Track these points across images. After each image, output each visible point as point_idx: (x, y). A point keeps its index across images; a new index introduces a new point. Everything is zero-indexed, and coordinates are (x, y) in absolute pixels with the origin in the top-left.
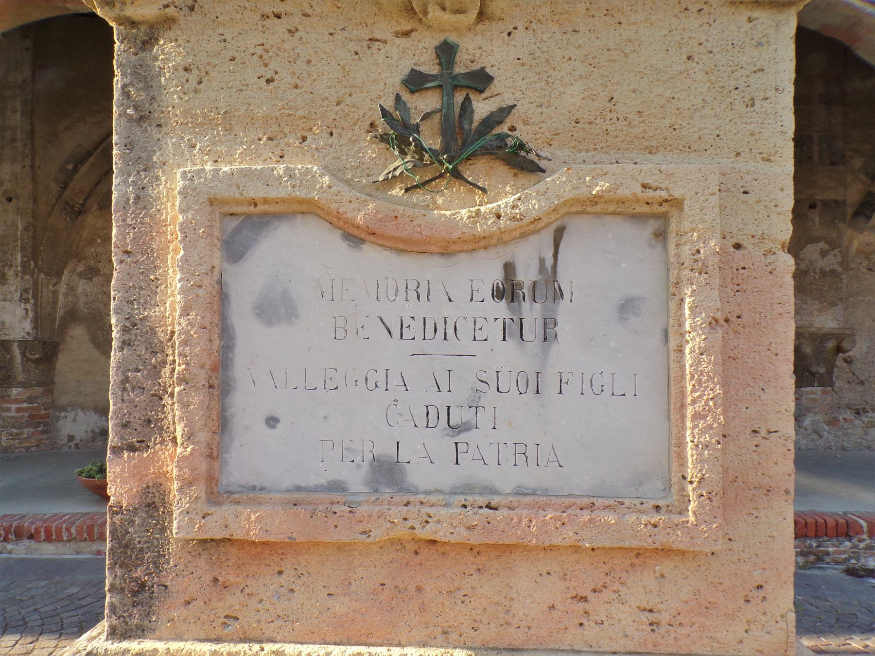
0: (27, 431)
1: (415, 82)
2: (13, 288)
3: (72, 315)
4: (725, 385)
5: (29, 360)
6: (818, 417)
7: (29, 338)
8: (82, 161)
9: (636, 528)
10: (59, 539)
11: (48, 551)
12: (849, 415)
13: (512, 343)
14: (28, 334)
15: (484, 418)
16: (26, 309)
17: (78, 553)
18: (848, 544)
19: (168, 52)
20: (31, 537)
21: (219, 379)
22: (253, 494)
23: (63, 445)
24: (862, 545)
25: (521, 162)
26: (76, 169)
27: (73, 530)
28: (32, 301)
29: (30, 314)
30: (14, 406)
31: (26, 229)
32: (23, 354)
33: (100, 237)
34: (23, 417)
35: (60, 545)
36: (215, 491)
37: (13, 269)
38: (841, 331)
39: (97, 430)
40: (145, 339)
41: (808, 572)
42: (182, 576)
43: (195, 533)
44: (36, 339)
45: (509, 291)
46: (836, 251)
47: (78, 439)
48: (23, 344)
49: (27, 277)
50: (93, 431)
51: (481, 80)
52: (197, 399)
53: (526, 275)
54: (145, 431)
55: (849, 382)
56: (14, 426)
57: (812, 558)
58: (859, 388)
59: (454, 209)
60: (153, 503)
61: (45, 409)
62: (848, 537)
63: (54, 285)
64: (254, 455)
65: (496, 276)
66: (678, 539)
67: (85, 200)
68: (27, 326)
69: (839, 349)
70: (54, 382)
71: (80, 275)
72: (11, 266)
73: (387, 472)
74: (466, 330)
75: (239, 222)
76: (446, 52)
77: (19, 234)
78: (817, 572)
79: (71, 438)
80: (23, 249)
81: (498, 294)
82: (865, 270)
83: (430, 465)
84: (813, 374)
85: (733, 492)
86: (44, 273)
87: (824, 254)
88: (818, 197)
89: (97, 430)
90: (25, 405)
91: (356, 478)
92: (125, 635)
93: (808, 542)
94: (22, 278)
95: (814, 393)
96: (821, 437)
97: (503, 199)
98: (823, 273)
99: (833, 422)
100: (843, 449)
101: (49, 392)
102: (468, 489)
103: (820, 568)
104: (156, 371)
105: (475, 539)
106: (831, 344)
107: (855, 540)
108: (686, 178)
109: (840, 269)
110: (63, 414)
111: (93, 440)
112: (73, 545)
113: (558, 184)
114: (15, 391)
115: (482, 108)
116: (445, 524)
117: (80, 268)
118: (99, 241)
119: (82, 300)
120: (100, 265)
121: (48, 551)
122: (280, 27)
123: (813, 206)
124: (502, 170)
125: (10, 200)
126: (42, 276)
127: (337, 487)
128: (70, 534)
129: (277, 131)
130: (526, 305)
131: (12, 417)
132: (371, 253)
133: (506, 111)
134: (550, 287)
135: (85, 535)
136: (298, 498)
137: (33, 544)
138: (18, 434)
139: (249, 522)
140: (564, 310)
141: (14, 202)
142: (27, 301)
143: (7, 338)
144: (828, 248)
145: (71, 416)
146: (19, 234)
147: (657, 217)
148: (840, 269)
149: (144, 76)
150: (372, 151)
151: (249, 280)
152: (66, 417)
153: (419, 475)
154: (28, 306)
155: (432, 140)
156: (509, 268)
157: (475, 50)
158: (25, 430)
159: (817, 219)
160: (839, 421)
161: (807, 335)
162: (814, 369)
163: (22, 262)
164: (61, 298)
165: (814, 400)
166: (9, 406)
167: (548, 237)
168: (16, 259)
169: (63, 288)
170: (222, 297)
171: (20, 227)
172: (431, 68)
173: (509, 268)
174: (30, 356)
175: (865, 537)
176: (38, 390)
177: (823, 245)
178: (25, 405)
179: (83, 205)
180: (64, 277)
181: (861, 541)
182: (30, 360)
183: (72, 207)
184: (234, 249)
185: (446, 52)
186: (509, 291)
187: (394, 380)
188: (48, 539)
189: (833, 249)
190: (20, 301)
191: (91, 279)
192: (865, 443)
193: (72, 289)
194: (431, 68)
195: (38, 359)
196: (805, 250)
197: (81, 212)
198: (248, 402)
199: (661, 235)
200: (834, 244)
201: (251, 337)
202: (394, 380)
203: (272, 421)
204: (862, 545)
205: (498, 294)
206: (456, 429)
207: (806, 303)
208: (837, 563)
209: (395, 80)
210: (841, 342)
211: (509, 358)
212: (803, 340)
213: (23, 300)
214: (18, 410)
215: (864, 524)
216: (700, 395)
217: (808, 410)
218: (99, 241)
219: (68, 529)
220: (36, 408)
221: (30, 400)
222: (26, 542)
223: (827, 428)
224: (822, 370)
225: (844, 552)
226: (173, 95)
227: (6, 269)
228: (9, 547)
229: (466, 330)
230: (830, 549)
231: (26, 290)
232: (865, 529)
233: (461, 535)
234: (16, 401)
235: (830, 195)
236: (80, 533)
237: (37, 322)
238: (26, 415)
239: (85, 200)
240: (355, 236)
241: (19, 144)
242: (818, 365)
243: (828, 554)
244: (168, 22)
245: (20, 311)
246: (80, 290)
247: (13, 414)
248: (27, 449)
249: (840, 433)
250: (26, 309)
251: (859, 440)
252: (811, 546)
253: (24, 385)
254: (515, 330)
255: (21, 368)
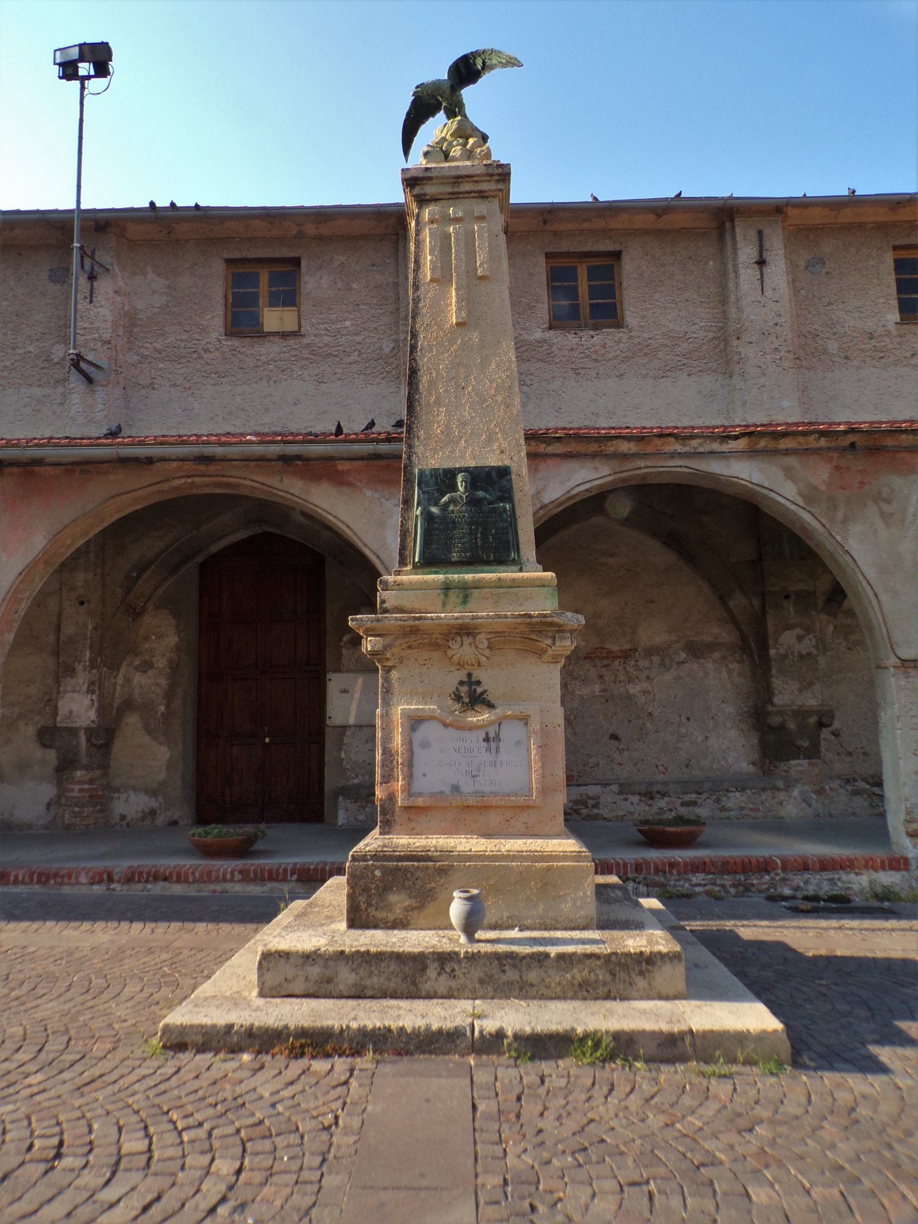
0: (87, 810)
1: (462, 683)
2: (81, 681)
3: (128, 705)
4: (542, 763)
5: (93, 745)
6: (807, 788)
7: (93, 726)
8: (144, 570)
9: (521, 800)
10: (186, 881)
11: (177, 889)
12: (835, 784)
13: (488, 753)
14: (93, 722)
15: (481, 774)
16: (92, 700)
17: (199, 891)
18: (767, 877)
19: (394, 674)
20: (165, 879)
21: (410, 764)
22: (420, 794)
23: (116, 824)
24: (778, 878)
25: (491, 706)
26: (139, 577)
27: (197, 875)
28: (97, 692)
29: (96, 704)
30: (77, 787)
31: (95, 628)
32: (88, 740)
33: (154, 634)
34: (84, 797)
35: (186, 886)
36: (410, 795)
37: (82, 664)
38: (820, 708)
39: (147, 810)
40: (388, 753)
41: (739, 899)
42: (399, 816)
43: (406, 804)
44: (99, 727)
45: (487, 740)
46: (811, 636)
47: (129, 818)
48: (89, 731)
49: (94, 671)
50: (143, 811)
51: (478, 683)
52: (405, 769)
53: (492, 735)
54: (388, 778)
55: (838, 754)
56: (76, 805)
57: (741, 889)
58: (848, 759)
59: (473, 719)
60: (391, 797)
61: (102, 790)
62: (767, 872)
63: (114, 678)
64: (419, 784)
65: (484, 735)
66: (531, 803)
67: (146, 603)
68: (92, 715)
69: (821, 725)
70: (109, 766)
71: (136, 668)
72: (80, 661)
73: (456, 788)
74: (476, 750)
75: (415, 722)
76: (469, 675)
77: (89, 633)
78: (745, 899)
79: (123, 817)
80: (91, 647)
81: (484, 740)
82: (844, 649)
83: (467, 787)
84: (799, 748)
85: (544, 791)
86: (107, 667)
87: (800, 639)
88: (790, 589)
89: (147, 810)
90: (86, 786)
91: (447, 790)
92: (384, 834)
93: (738, 877)
94: (90, 672)
95: (801, 765)
96: (810, 805)
97: (484, 716)
98: (801, 656)
99: (820, 792)
100: (831, 815)
101: (106, 774)
102: (477, 792)
103: (748, 896)
104: (392, 762)
105: (479, 804)
106: (812, 720)
107: (772, 875)
108: (532, 710)
109: (815, 652)
110: (116, 795)
111: (143, 819)
112: (196, 886)
113: (499, 711)
114: (79, 773)
115: (479, 690)
116: (471, 801)
117: (137, 662)
118: (154, 638)
119: (137, 691)
120: (154, 660)
121: (177, 889)
122: (425, 667)
123: (787, 597)
124: (485, 707)
125: (82, 603)
126: (105, 669)
127: (442, 792)
128: (195, 877)
129: (425, 697)
130: (492, 743)
131: (76, 797)
132: (450, 730)
133: (485, 691)
134: (497, 738)
135: (205, 878)
136: (432, 795)
137: (166, 884)
138: (80, 813)
139: (420, 802)
140: (501, 744)
141: (86, 605)
142: (93, 692)
143: (74, 725)
144: (803, 633)
145: (123, 797)
146: (89, 633)
147: (525, 720)
148: (815, 652)
149: (387, 680)
150: (450, 702)
151: (418, 736)
152: (119, 798)
153: (465, 789)
154: (94, 697)
155: (467, 700)
156: (487, 734)
157: (478, 674)
158: (86, 809)
159: (791, 608)
160: (826, 790)
161: (789, 713)
162: (799, 743)
163: (90, 657)
164: (118, 688)
165: (802, 772)
166: (72, 787)
167: (497, 725)
168: (85, 655)
169: (120, 680)
170: (411, 742)
171: (90, 627)
172: (466, 680)
173: (487, 734)
174: (95, 742)
175: (780, 871)
176: (97, 773)
177: (798, 631)
178: (86, 786)
179: (143, 607)
180: (123, 670)
181: (777, 874)
182: (95, 746)
183: (135, 609)
184: (413, 728)
185: (469, 675)
186: (487, 740)
187: (457, 764)
188: (178, 881)
189: (808, 634)
190: (88, 692)
191: (145, 672)
192: (850, 810)
193: (128, 681)
194: (466, 680)
195: (102, 744)
196: (783, 635)
197: (140, 614)
198: (418, 770)
199: (526, 724)
200: (808, 630)
201: (418, 751)
202: (457, 764)
203: (424, 775)
204: (778, 878)
205: (484, 740)
206: (474, 777)
207: (787, 683)
208: (760, 892)
209: (455, 683)
210: (821, 718)
211: (486, 757)
212: (787, 717)
213: (90, 691)
214: (81, 790)
215: (778, 861)
216: (536, 766)
217: (797, 781)
218: (154, 638)
219: (193, 874)
220: (96, 790)
221: (91, 781)
222: (161, 884)
223: (814, 796)
224: (806, 744)
225: (765, 883)
226: (396, 685)
227: (76, 664)
228: (149, 886)
229: (476, 750)
230: (755, 882)
231: (93, 683)
232: (780, 866)
233: (475, 804)
234: (79, 782)
235: (801, 586)
236: (201, 876)
237: (102, 710)
238: (87, 795)
239: (146, 603)
240: (446, 725)
241: (92, 556)
242: (802, 739)
243: (753, 885)
244: (394, 667)
245: (86, 701)
246: (136, 681)
247: (76, 794)
248: (87, 826)
249: (827, 802)
250: (92, 700)
251: (844, 808)
252: (740, 880)
253: (87, 768)
254: (489, 750)
255: (85, 753)
